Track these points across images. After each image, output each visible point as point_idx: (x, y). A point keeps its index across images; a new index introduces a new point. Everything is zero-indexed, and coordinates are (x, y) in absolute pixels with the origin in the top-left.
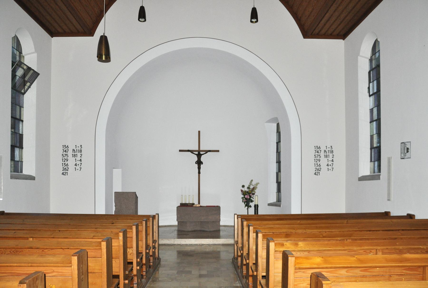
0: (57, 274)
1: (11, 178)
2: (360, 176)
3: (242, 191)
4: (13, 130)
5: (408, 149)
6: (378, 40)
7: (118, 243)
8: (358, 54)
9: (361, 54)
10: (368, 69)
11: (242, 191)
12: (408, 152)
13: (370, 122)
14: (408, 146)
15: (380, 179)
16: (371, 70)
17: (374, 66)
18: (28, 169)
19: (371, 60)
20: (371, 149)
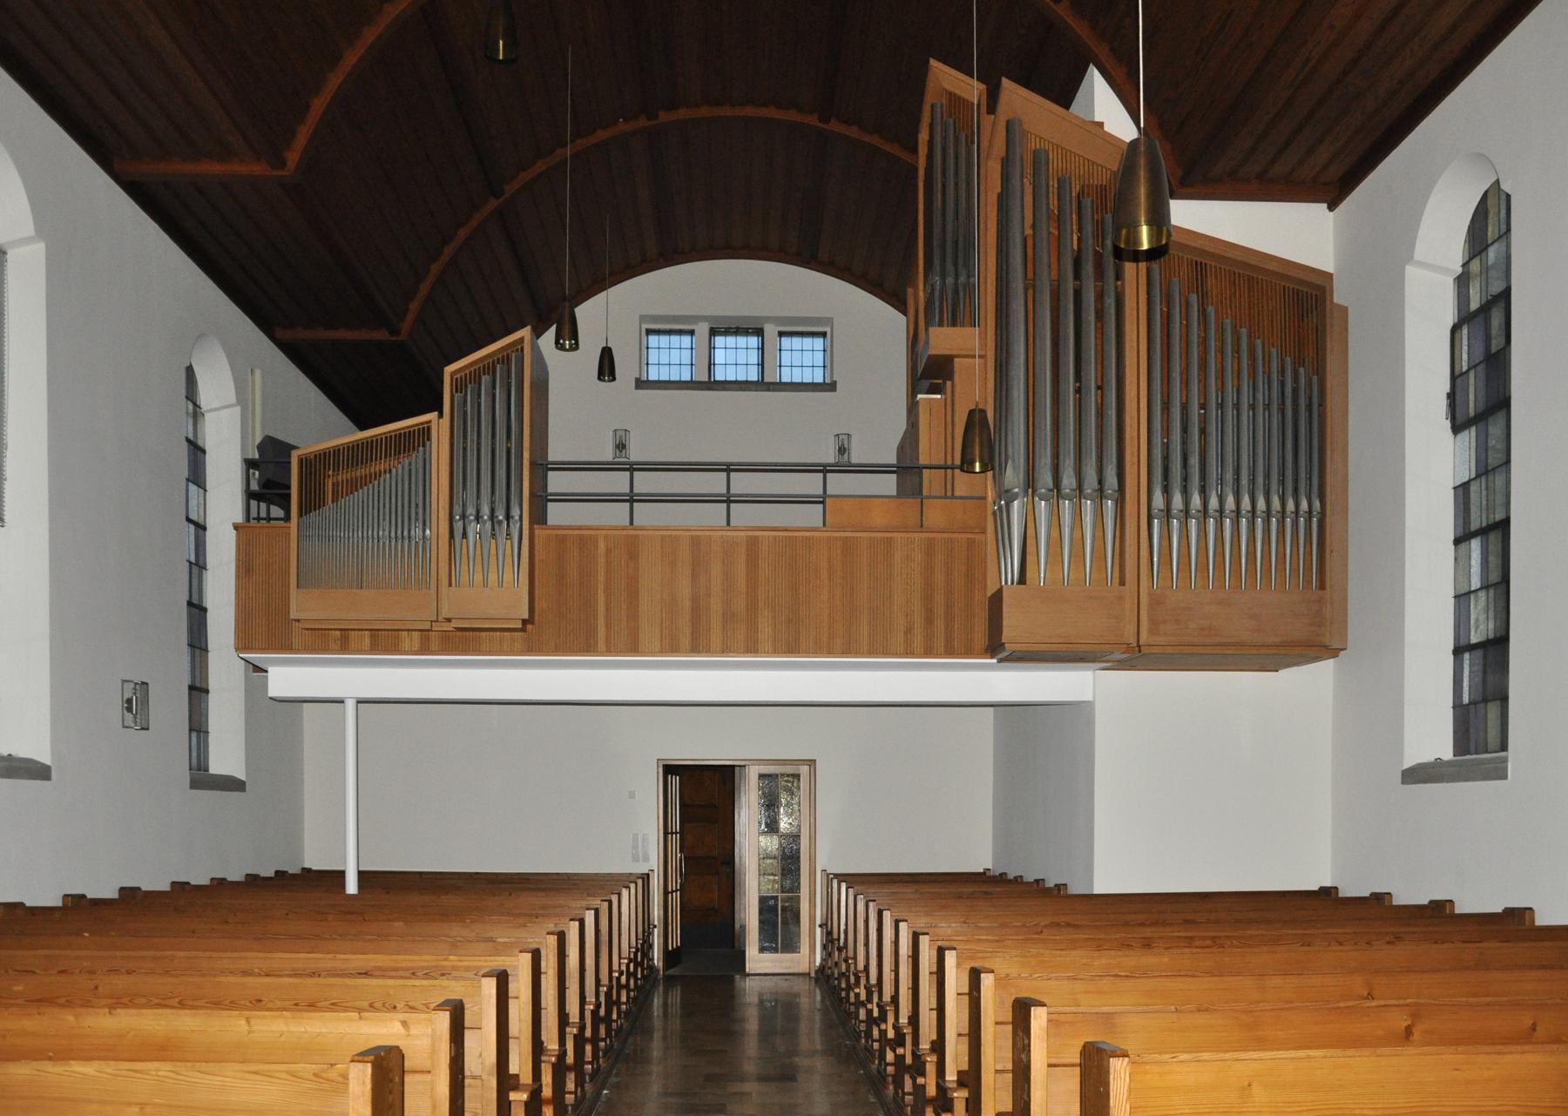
0: (1142, 161)
1: (192, 787)
2: (1406, 766)
3: (295, 448)
4: (407, 640)
5: (129, 709)
6: (1505, 187)
7: (589, 917)
8: (1409, 258)
9: (1419, 254)
10: (1449, 316)
11: (295, 448)
12: (129, 701)
13: (1457, 542)
14: (129, 716)
15: (1505, 777)
16: (1465, 319)
17: (1474, 305)
18: (225, 758)
19: (1462, 281)
20: (1458, 651)
